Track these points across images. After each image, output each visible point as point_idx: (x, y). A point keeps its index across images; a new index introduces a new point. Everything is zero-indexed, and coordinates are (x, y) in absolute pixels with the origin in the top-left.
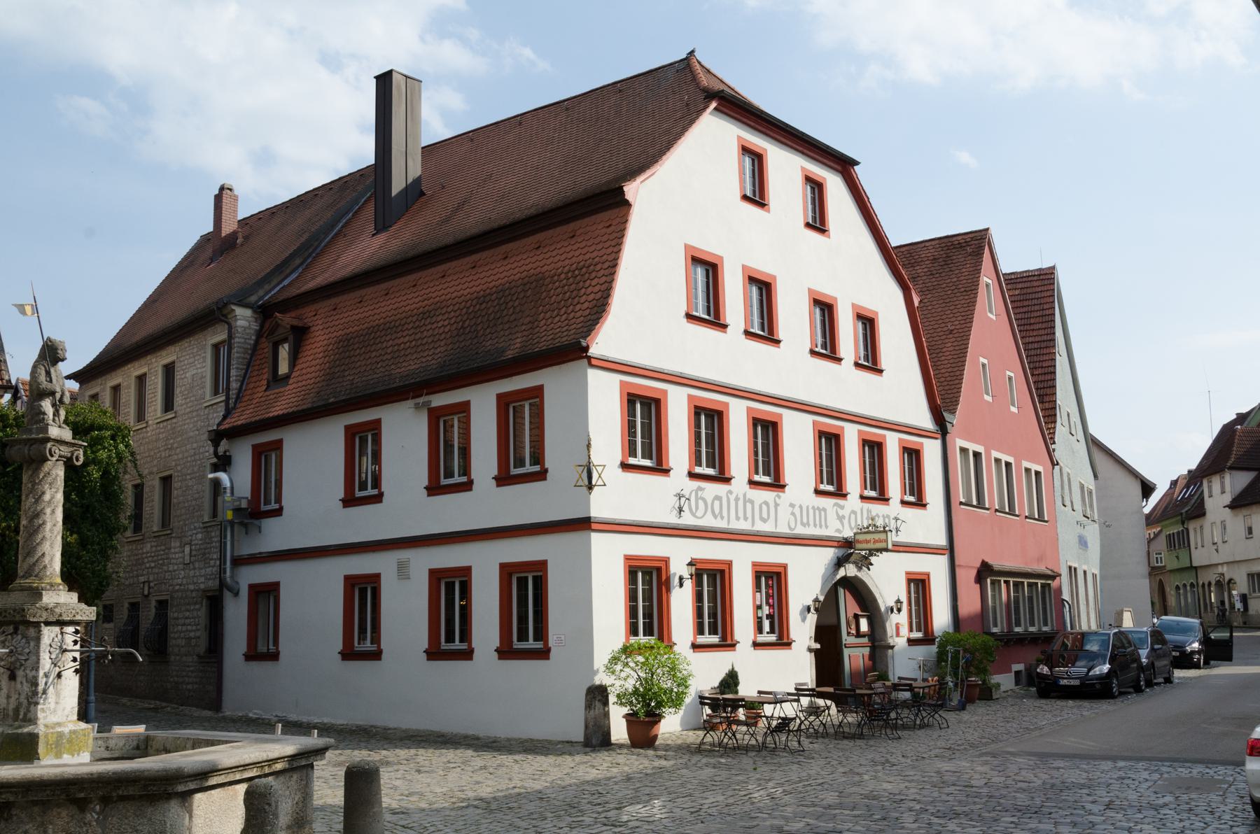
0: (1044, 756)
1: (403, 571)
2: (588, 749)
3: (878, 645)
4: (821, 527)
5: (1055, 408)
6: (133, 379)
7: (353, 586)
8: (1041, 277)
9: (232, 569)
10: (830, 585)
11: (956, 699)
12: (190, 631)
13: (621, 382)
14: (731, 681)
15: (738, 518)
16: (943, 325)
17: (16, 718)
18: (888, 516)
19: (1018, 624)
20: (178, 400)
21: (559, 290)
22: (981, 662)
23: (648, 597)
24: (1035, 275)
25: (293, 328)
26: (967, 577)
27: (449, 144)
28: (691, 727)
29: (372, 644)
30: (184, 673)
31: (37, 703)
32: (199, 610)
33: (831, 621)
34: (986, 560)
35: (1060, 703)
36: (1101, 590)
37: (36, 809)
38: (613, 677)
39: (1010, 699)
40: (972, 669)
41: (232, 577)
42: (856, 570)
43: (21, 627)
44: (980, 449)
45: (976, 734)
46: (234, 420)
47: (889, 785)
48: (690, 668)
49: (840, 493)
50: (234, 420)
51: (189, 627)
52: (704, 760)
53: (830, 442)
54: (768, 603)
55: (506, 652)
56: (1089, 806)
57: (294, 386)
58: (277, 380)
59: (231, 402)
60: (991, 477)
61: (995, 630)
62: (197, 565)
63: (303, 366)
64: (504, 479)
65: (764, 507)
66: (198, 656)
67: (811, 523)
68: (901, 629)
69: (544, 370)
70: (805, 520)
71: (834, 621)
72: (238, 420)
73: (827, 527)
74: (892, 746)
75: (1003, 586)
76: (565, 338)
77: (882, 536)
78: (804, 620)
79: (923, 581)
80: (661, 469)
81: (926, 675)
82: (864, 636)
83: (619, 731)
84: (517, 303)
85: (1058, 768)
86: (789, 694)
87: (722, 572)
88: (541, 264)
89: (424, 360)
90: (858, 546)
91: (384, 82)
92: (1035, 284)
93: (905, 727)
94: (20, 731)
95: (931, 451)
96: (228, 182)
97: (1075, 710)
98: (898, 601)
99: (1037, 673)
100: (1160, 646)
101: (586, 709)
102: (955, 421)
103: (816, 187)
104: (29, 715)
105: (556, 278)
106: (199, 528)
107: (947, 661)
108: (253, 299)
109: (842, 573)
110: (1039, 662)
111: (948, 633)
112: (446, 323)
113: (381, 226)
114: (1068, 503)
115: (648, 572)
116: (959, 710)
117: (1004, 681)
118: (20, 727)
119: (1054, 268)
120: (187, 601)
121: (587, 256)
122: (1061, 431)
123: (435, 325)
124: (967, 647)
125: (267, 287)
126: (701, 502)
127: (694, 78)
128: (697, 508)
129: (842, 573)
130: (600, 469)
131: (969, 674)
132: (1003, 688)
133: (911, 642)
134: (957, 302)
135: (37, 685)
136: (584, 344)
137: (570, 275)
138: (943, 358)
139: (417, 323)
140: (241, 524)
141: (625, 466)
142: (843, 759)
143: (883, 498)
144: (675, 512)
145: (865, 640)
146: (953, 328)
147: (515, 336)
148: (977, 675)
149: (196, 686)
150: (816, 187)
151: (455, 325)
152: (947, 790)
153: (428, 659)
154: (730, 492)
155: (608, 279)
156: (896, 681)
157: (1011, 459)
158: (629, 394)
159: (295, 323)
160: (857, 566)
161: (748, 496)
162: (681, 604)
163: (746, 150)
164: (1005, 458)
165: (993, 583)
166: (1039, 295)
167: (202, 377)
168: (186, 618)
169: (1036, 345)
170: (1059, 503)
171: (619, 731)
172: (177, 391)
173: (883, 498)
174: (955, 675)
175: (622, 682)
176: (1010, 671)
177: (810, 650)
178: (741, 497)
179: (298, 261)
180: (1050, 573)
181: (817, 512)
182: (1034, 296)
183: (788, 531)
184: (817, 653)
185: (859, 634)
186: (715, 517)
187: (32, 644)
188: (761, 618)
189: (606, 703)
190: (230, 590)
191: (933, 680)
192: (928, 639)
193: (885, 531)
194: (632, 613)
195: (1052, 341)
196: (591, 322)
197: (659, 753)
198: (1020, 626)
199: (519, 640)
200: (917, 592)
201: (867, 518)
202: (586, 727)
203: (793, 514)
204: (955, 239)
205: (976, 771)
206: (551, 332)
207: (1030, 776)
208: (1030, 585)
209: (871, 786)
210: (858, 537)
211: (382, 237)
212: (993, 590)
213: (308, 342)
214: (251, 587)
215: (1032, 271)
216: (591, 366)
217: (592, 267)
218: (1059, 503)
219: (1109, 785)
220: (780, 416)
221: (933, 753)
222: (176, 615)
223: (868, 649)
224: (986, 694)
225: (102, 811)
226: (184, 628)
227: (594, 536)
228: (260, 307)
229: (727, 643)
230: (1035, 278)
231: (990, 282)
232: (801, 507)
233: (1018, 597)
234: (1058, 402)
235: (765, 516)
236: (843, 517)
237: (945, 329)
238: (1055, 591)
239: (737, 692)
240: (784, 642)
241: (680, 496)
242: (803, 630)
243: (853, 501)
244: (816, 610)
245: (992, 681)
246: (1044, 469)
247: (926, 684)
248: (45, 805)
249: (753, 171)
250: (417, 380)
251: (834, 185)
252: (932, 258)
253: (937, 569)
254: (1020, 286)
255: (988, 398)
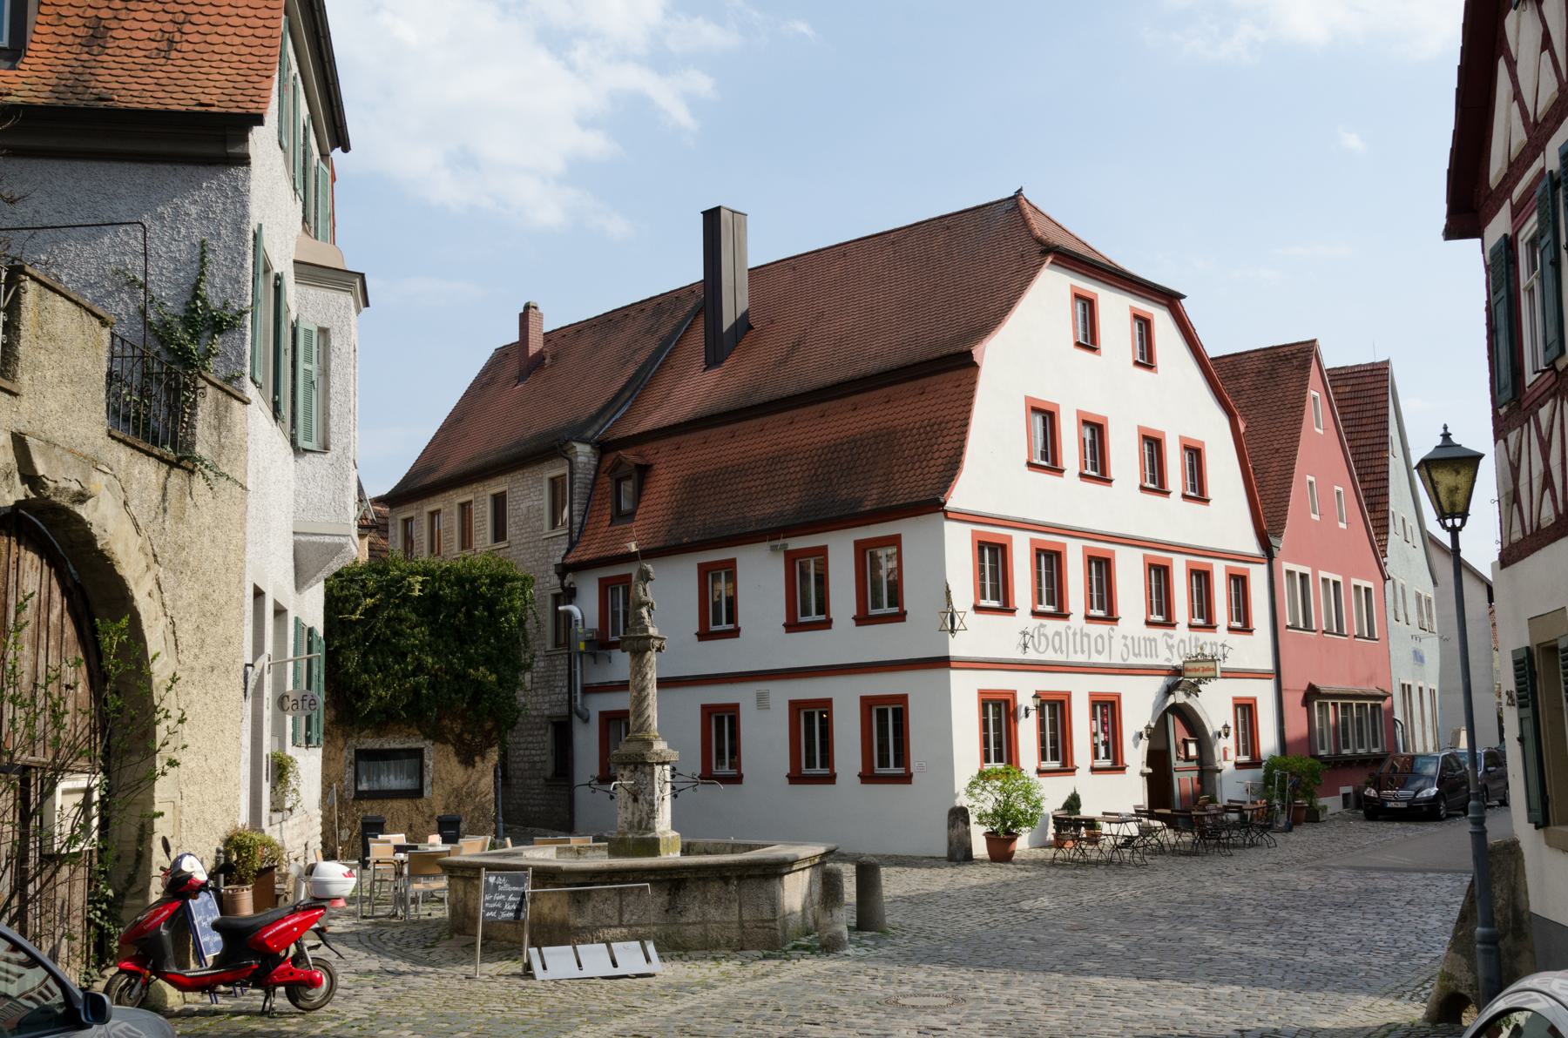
0: (1362, 870)
1: (762, 701)
2: (953, 863)
3: (1206, 769)
4: (1151, 656)
5: (1387, 518)
6: (456, 506)
7: (710, 714)
8: (1374, 373)
9: (582, 697)
10: (1160, 713)
11: (1283, 820)
12: (534, 755)
13: (973, 531)
14: (1073, 803)
15: (1076, 652)
16: (1269, 443)
17: (640, 827)
18: (1215, 644)
19: (1346, 746)
20: (511, 530)
21: (912, 444)
22: (1308, 785)
23: (997, 724)
24: (1367, 371)
25: (637, 466)
26: (1294, 700)
27: (772, 270)
28: (1037, 845)
29: (730, 768)
30: (529, 796)
31: (654, 818)
32: (544, 735)
33: (1160, 746)
34: (1313, 683)
35: (1387, 825)
36: (1441, 708)
37: (700, 883)
38: (973, 799)
39: (1336, 822)
40: (1298, 792)
41: (582, 704)
42: (1184, 697)
43: (640, 766)
44: (1307, 570)
45: (1302, 852)
46: (579, 554)
47: (1228, 889)
48: (1041, 792)
49: (1169, 623)
50: (579, 554)
51: (533, 752)
52: (1062, 872)
53: (1159, 574)
54: (1103, 730)
55: (868, 777)
56: (1392, 903)
57: (640, 522)
58: (620, 516)
59: (575, 535)
60: (1317, 595)
61: (1322, 753)
62: (540, 692)
63: (649, 502)
64: (862, 619)
65: (1099, 640)
66: (546, 780)
67: (1143, 652)
68: (1228, 754)
69: (907, 520)
70: (1137, 651)
71: (1164, 747)
72: (582, 554)
73: (1157, 656)
74: (1225, 861)
75: (1331, 708)
76: (922, 493)
77: (1211, 665)
78: (1136, 745)
79: (1250, 706)
80: (1007, 609)
81: (1254, 798)
82: (1192, 760)
83: (980, 847)
84: (870, 454)
85: (1373, 879)
86: (1133, 815)
87: (1062, 702)
88: (892, 418)
89: (778, 504)
90: (1187, 674)
91: (712, 218)
92: (1367, 380)
93: (1235, 846)
94: (645, 836)
95: (1258, 577)
96: (533, 301)
97: (1400, 832)
98: (1226, 727)
99: (1365, 796)
100: (1493, 768)
101: (949, 828)
102: (1282, 544)
103: (1144, 325)
104: (649, 826)
105: (908, 433)
106: (541, 656)
107: (1273, 784)
108: (590, 434)
109: (1171, 700)
110: (1368, 784)
111: (1274, 757)
112: (798, 469)
113: (713, 361)
114: (1401, 617)
115: (997, 704)
116: (1286, 832)
117: (1331, 804)
118: (643, 834)
119: (1387, 362)
120: (529, 726)
121: (938, 414)
122: (1394, 539)
123: (786, 471)
124: (1294, 770)
125: (601, 422)
126: (1043, 638)
127: (1026, 222)
128: (1040, 644)
129: (1171, 700)
130: (961, 615)
131: (1295, 797)
132: (1330, 811)
133: (1238, 765)
134: (1283, 420)
135: (654, 805)
136: (942, 500)
137: (922, 430)
138: (1269, 478)
139: (768, 468)
140: (590, 654)
141: (978, 609)
142: (1184, 871)
143: (1210, 626)
144: (1021, 649)
145: (1194, 764)
146: (1279, 446)
147: (870, 488)
148: (1302, 797)
149: (542, 808)
150: (1144, 325)
151: (807, 472)
152: (1278, 892)
153: (790, 783)
154: (1069, 627)
155: (961, 437)
156: (1226, 803)
157: (1339, 578)
158: (979, 542)
159: (639, 461)
160: (1186, 693)
161: (1085, 631)
162: (1027, 733)
163: (1077, 297)
164: (1332, 577)
165: (1320, 705)
166: (1370, 393)
167: (539, 510)
168: (530, 743)
169: (1368, 449)
170: (1391, 618)
171: (980, 847)
172: (509, 521)
173: (1210, 626)
174: (1282, 797)
175: (981, 805)
176: (1338, 794)
177: (1143, 774)
178: (1078, 631)
179: (627, 394)
180: (1380, 693)
181: (1148, 643)
182: (1365, 394)
183: (1121, 662)
184: (1149, 777)
185: (1187, 759)
186: (1056, 651)
187: (649, 778)
188: (1096, 745)
189: (967, 823)
190: (580, 716)
191: (1261, 803)
192: (1255, 763)
193: (1213, 660)
194: (985, 742)
195: (1384, 444)
196: (945, 479)
197: (1019, 866)
198: (1348, 748)
199: (880, 766)
200: (1244, 716)
201: (1196, 646)
202: (950, 843)
203: (1126, 645)
204: (1280, 350)
205: (1303, 880)
206: (906, 486)
207: (1350, 884)
208: (1359, 706)
209: (1213, 890)
210: (1187, 665)
211: (714, 374)
212: (1320, 712)
213: (652, 479)
214: (602, 714)
215: (1364, 365)
216: (947, 518)
217: (943, 425)
218: (1391, 618)
219: (1415, 889)
220: (1113, 552)
221: (1263, 867)
222: (517, 740)
223: (1196, 773)
224: (1313, 816)
225: (738, 884)
226: (527, 752)
227: (953, 673)
228: (598, 442)
229: (1068, 769)
230: (1368, 374)
231: (1317, 394)
232: (1133, 638)
233: (1346, 719)
234: (1391, 509)
235: (1100, 648)
236: (1173, 646)
237: (1271, 447)
238: (1386, 712)
239: (1079, 813)
240: (1118, 767)
241: (1024, 634)
242: (1135, 755)
243: (1182, 630)
244: (1148, 736)
245: (1319, 804)
246: (1375, 586)
247: (1255, 806)
248: (705, 880)
249: (1085, 316)
250: (774, 525)
251: (1161, 319)
252: (1256, 371)
253: (1264, 694)
254: (1351, 382)
255: (1315, 517)
